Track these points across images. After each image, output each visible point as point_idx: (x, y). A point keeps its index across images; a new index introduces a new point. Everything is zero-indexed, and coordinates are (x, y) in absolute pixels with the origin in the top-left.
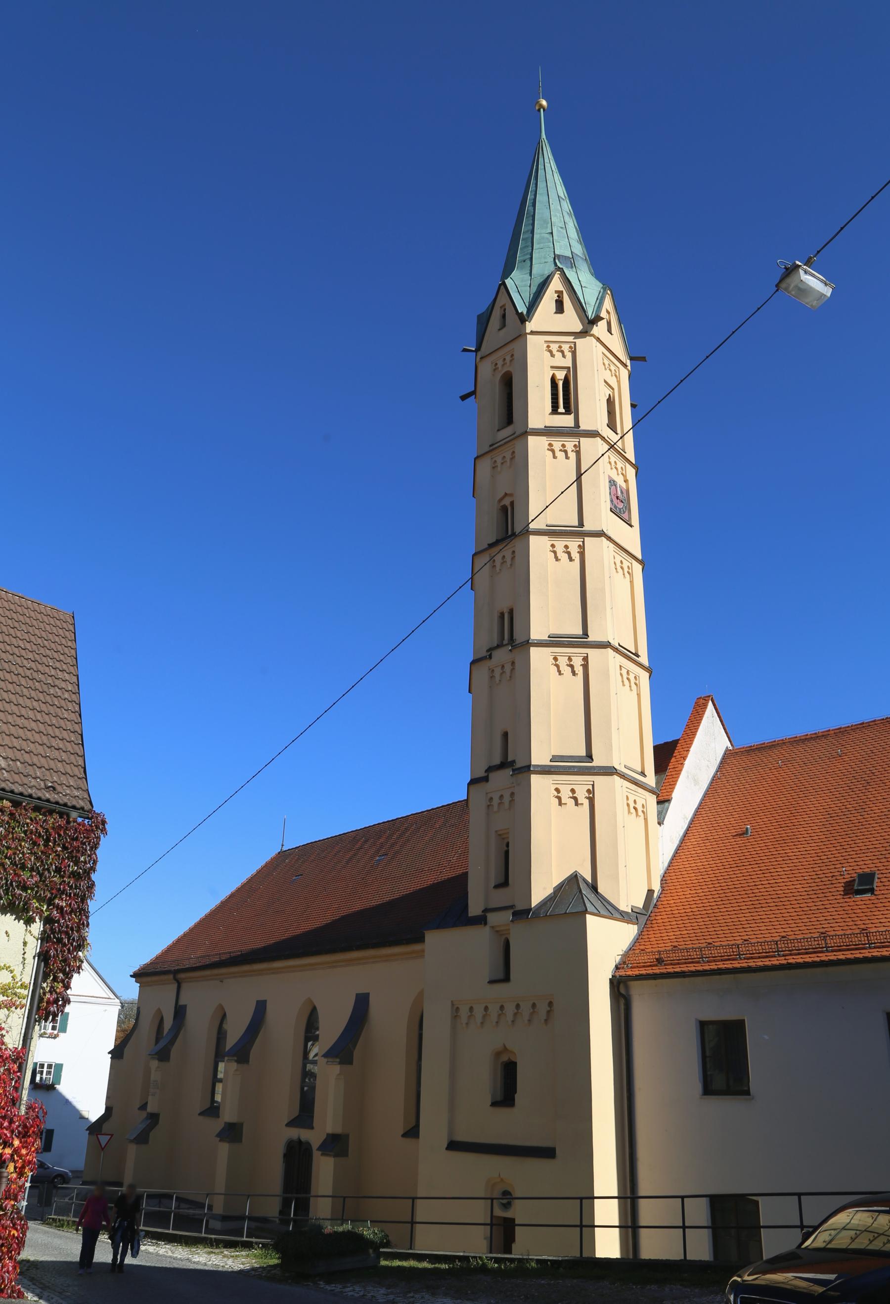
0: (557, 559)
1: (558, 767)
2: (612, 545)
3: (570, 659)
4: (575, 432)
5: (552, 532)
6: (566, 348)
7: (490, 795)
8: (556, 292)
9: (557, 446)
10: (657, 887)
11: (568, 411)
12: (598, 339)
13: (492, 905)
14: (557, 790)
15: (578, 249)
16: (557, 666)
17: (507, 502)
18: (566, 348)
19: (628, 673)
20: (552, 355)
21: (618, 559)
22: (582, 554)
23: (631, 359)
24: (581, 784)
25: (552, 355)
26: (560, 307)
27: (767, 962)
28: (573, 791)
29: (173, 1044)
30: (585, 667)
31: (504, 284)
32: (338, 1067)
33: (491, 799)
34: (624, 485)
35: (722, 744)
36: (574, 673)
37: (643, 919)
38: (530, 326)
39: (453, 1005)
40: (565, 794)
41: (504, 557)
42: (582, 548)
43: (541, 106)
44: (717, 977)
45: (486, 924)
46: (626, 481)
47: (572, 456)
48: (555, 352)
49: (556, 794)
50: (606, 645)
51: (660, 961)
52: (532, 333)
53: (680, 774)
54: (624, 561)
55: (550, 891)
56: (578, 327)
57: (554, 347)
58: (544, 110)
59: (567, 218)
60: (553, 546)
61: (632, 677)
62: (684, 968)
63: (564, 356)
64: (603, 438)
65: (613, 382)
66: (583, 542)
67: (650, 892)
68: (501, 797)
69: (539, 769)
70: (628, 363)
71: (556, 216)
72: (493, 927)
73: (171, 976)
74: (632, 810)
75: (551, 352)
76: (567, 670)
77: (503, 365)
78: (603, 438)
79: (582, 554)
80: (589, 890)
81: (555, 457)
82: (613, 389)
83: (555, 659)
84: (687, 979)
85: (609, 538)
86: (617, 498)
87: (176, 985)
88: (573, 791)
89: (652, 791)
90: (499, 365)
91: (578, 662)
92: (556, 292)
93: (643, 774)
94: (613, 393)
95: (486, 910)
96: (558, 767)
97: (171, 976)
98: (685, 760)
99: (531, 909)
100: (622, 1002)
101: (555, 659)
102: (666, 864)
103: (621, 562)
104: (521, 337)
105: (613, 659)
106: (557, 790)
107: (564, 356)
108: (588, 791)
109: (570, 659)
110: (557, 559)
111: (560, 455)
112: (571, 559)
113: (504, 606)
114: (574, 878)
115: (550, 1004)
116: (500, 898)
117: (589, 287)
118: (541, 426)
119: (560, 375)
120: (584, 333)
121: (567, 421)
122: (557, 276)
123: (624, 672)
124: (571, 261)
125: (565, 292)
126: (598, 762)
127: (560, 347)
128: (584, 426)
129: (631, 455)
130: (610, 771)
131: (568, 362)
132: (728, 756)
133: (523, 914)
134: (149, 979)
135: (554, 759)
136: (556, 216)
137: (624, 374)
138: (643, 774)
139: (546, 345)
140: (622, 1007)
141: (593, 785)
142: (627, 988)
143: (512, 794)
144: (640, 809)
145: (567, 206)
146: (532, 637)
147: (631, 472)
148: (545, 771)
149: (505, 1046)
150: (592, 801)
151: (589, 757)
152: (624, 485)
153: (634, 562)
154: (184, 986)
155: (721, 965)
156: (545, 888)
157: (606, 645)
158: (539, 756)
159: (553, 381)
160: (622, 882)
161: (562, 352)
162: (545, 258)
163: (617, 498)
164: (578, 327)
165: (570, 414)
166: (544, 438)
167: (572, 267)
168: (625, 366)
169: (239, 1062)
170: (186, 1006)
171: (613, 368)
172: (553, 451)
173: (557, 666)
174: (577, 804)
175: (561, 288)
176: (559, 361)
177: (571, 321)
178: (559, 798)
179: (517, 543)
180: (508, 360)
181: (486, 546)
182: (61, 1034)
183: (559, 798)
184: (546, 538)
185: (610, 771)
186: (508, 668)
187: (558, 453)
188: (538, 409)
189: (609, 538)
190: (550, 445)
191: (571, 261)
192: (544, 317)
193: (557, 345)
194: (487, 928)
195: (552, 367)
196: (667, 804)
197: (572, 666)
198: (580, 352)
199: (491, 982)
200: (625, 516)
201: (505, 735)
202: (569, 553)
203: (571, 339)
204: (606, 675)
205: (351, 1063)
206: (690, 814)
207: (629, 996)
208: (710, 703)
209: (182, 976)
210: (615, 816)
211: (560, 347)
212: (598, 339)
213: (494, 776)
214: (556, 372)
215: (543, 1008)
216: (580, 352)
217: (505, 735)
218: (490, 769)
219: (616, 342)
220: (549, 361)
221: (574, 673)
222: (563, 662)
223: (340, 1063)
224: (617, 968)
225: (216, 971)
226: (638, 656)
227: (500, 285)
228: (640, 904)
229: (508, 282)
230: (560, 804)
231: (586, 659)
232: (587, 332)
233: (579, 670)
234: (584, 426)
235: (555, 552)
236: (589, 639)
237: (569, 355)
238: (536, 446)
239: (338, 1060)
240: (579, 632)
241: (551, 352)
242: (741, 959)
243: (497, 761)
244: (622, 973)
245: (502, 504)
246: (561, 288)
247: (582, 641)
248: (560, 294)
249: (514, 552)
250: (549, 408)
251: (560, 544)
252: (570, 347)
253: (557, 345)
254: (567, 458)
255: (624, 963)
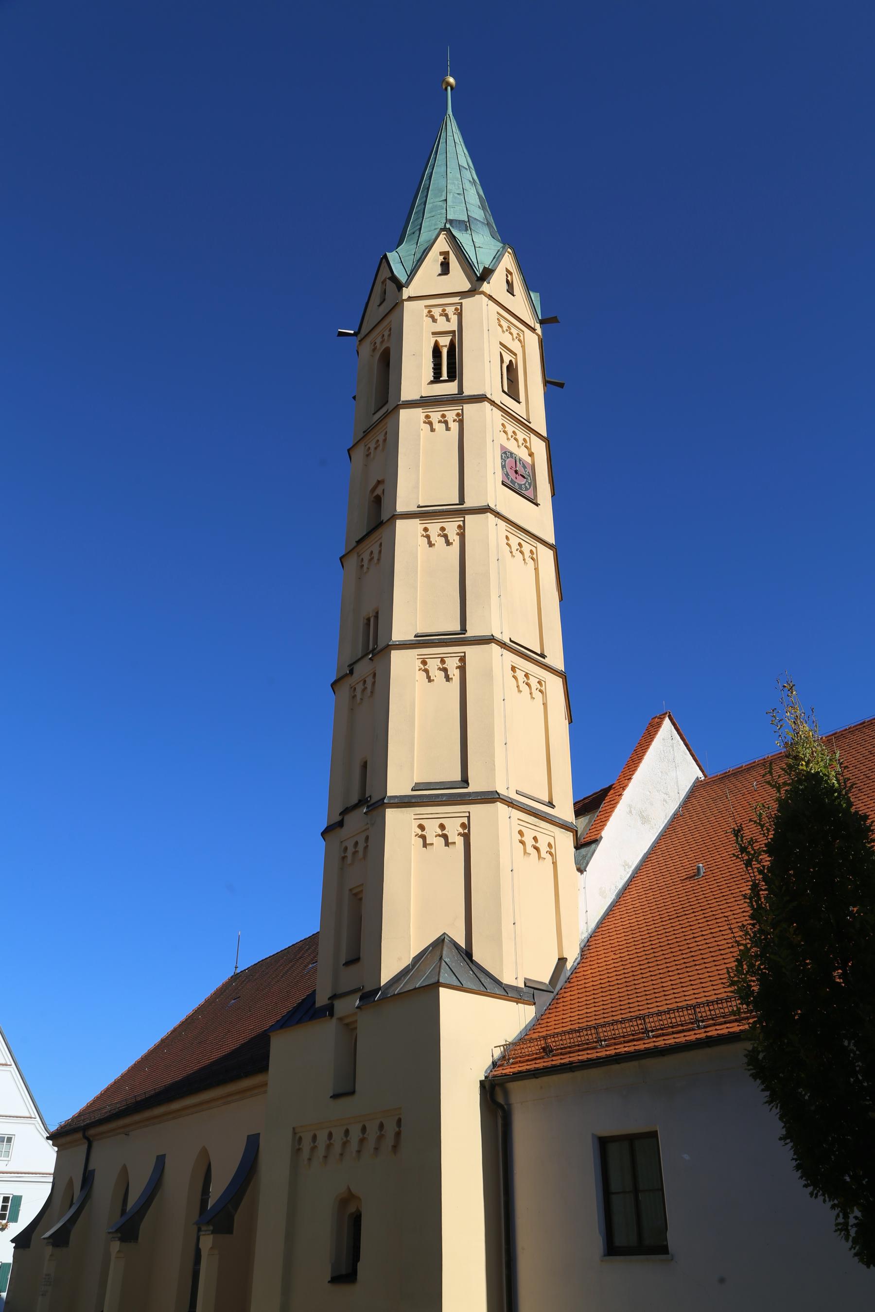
0: (431, 544)
1: (421, 798)
2: (502, 524)
3: (443, 661)
4: (459, 399)
5: (425, 514)
6: (450, 310)
7: (344, 845)
8: (441, 253)
9: (435, 417)
10: (572, 955)
11: (452, 377)
12: (490, 297)
13: (340, 991)
14: (422, 827)
15: (478, 214)
16: (426, 671)
17: (378, 491)
18: (450, 310)
19: (527, 675)
20: (434, 321)
21: (514, 541)
22: (462, 536)
23: (542, 322)
24: (452, 817)
25: (434, 321)
26: (445, 268)
27: (681, 1039)
28: (442, 827)
29: (75, 1222)
30: (462, 669)
31: (385, 257)
32: (212, 1236)
33: (346, 849)
34: (528, 460)
35: (688, 773)
36: (448, 678)
37: (545, 999)
38: (406, 293)
39: (295, 1133)
40: (432, 829)
41: (372, 552)
42: (462, 529)
43: (448, 84)
44: (616, 1067)
45: (332, 1015)
46: (531, 455)
47: (454, 426)
48: (437, 316)
49: (420, 832)
50: (489, 640)
51: (547, 1050)
52: (410, 299)
53: (614, 807)
54: (510, 535)
55: (407, 961)
56: (466, 286)
57: (436, 312)
58: (452, 89)
59: (467, 185)
60: (426, 530)
61: (533, 682)
62: (575, 1058)
63: (448, 320)
64: (493, 403)
65: (515, 346)
66: (464, 521)
67: (562, 961)
68: (356, 843)
69: (396, 801)
70: (538, 327)
71: (453, 183)
72: (340, 1019)
73: (79, 1135)
74: (530, 849)
75: (432, 317)
76: (438, 676)
77: (382, 342)
78: (493, 403)
79: (462, 536)
80: (457, 957)
81: (432, 430)
82: (515, 355)
83: (424, 663)
84: (578, 1074)
85: (497, 514)
86: (516, 472)
87: (85, 1147)
88: (442, 827)
89: (565, 826)
90: (378, 345)
91: (452, 664)
92: (441, 253)
93: (551, 804)
94: (516, 360)
95: (334, 997)
96: (421, 798)
97: (79, 1135)
98: (624, 790)
99: (380, 989)
100: (500, 1113)
101: (424, 663)
102: (592, 925)
103: (520, 544)
104: (397, 306)
105: (505, 659)
106: (422, 827)
107: (448, 320)
108: (463, 825)
109: (443, 661)
110: (431, 544)
111: (439, 427)
112: (448, 543)
113: (367, 610)
114: (440, 942)
115: (399, 1121)
116: (350, 978)
117: (482, 245)
118: (416, 397)
119: (445, 341)
120: (472, 292)
121: (451, 388)
122: (442, 237)
123: (520, 675)
124: (466, 225)
125: (451, 253)
126: (475, 785)
127: (444, 310)
128: (467, 392)
129: (540, 423)
130: (490, 797)
131: (453, 326)
132: (697, 788)
133: (370, 995)
134: (69, 1139)
135: (417, 787)
136: (453, 183)
137: (532, 341)
138: (551, 804)
139: (426, 311)
140: (500, 1122)
141: (469, 817)
142: (506, 1093)
143: (367, 838)
144: (544, 849)
145: (470, 174)
146: (394, 639)
147: (540, 448)
148: (404, 802)
149: (349, 1188)
150: (467, 837)
151: (465, 781)
152: (528, 460)
153: (540, 546)
154: (95, 1144)
155: (622, 1049)
156: (400, 959)
157: (489, 640)
158: (397, 784)
159: (437, 352)
160: (507, 946)
161: (446, 316)
162: (436, 225)
163: (516, 472)
164: (466, 286)
165: (453, 381)
166: (420, 410)
167: (466, 230)
168: (533, 330)
169: (122, 1240)
170: (94, 1170)
171: (515, 331)
172: (431, 424)
173: (426, 671)
174: (447, 844)
175: (446, 248)
176: (442, 325)
177: (458, 280)
178: (423, 837)
179: (383, 532)
180: (386, 337)
181: (354, 544)
182: (11, 1225)
183: (423, 837)
184: (417, 521)
185: (490, 797)
186: (369, 681)
187: (436, 426)
188: (415, 376)
189: (497, 514)
190: (427, 417)
191: (466, 225)
192: (426, 279)
193: (440, 310)
194: (334, 1020)
195: (433, 333)
196: (593, 846)
197: (445, 670)
198: (474, 320)
199: (335, 1096)
200: (529, 493)
201: (365, 766)
202: (446, 536)
203: (456, 300)
204: (488, 675)
205: (229, 1230)
206: (635, 860)
207: (509, 1105)
208: (667, 719)
209: (92, 1132)
210: (498, 856)
211: (444, 310)
212: (490, 297)
213: (350, 819)
214: (438, 339)
215: (391, 1129)
216: (474, 320)
217: (365, 766)
218: (346, 812)
219: (520, 303)
220: (429, 326)
221: (448, 678)
222: (434, 665)
223: (213, 1232)
224: (494, 1064)
225: (121, 1122)
226: (543, 656)
227: (382, 259)
228: (544, 976)
229: (392, 256)
230: (425, 845)
231: (463, 659)
232: (475, 290)
233: (455, 674)
234: (467, 392)
235: (428, 537)
236: (468, 634)
237: (454, 318)
238: (410, 421)
239: (211, 1228)
240: (457, 628)
241: (432, 317)
242: (649, 1037)
243: (354, 800)
244: (499, 1072)
245: (375, 494)
246: (446, 248)
247: (459, 638)
248: (445, 254)
249: (381, 544)
250: (430, 375)
251: (434, 528)
252: (456, 309)
253: (440, 310)
254: (448, 429)
255: (504, 1057)
